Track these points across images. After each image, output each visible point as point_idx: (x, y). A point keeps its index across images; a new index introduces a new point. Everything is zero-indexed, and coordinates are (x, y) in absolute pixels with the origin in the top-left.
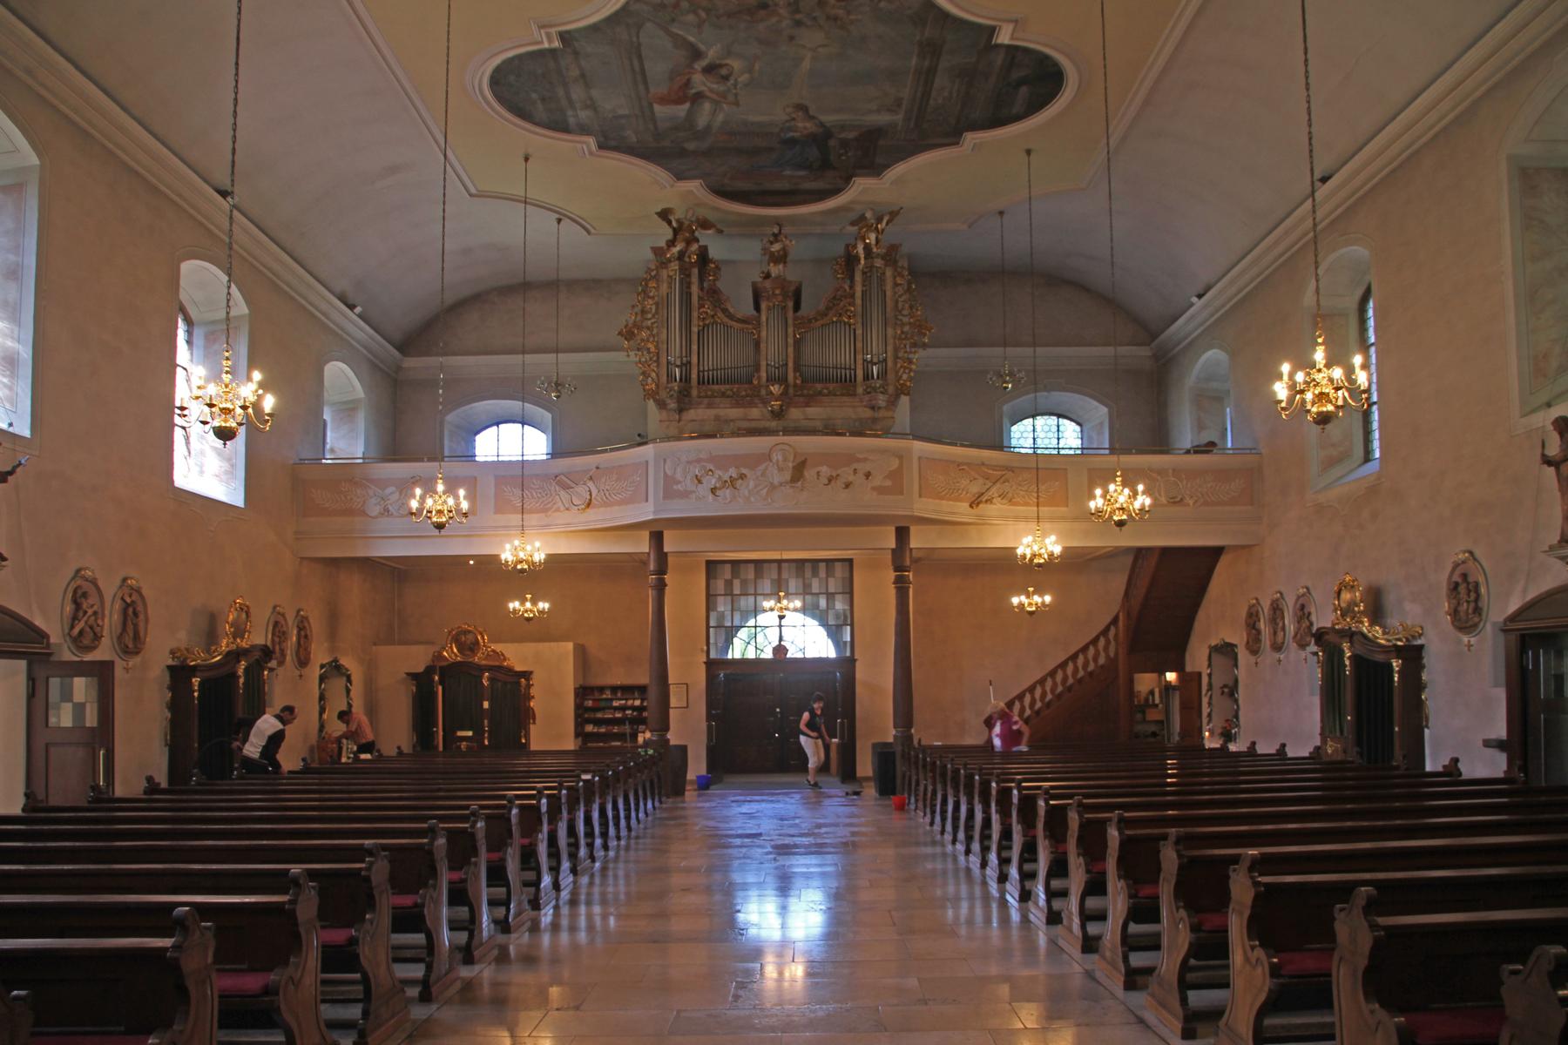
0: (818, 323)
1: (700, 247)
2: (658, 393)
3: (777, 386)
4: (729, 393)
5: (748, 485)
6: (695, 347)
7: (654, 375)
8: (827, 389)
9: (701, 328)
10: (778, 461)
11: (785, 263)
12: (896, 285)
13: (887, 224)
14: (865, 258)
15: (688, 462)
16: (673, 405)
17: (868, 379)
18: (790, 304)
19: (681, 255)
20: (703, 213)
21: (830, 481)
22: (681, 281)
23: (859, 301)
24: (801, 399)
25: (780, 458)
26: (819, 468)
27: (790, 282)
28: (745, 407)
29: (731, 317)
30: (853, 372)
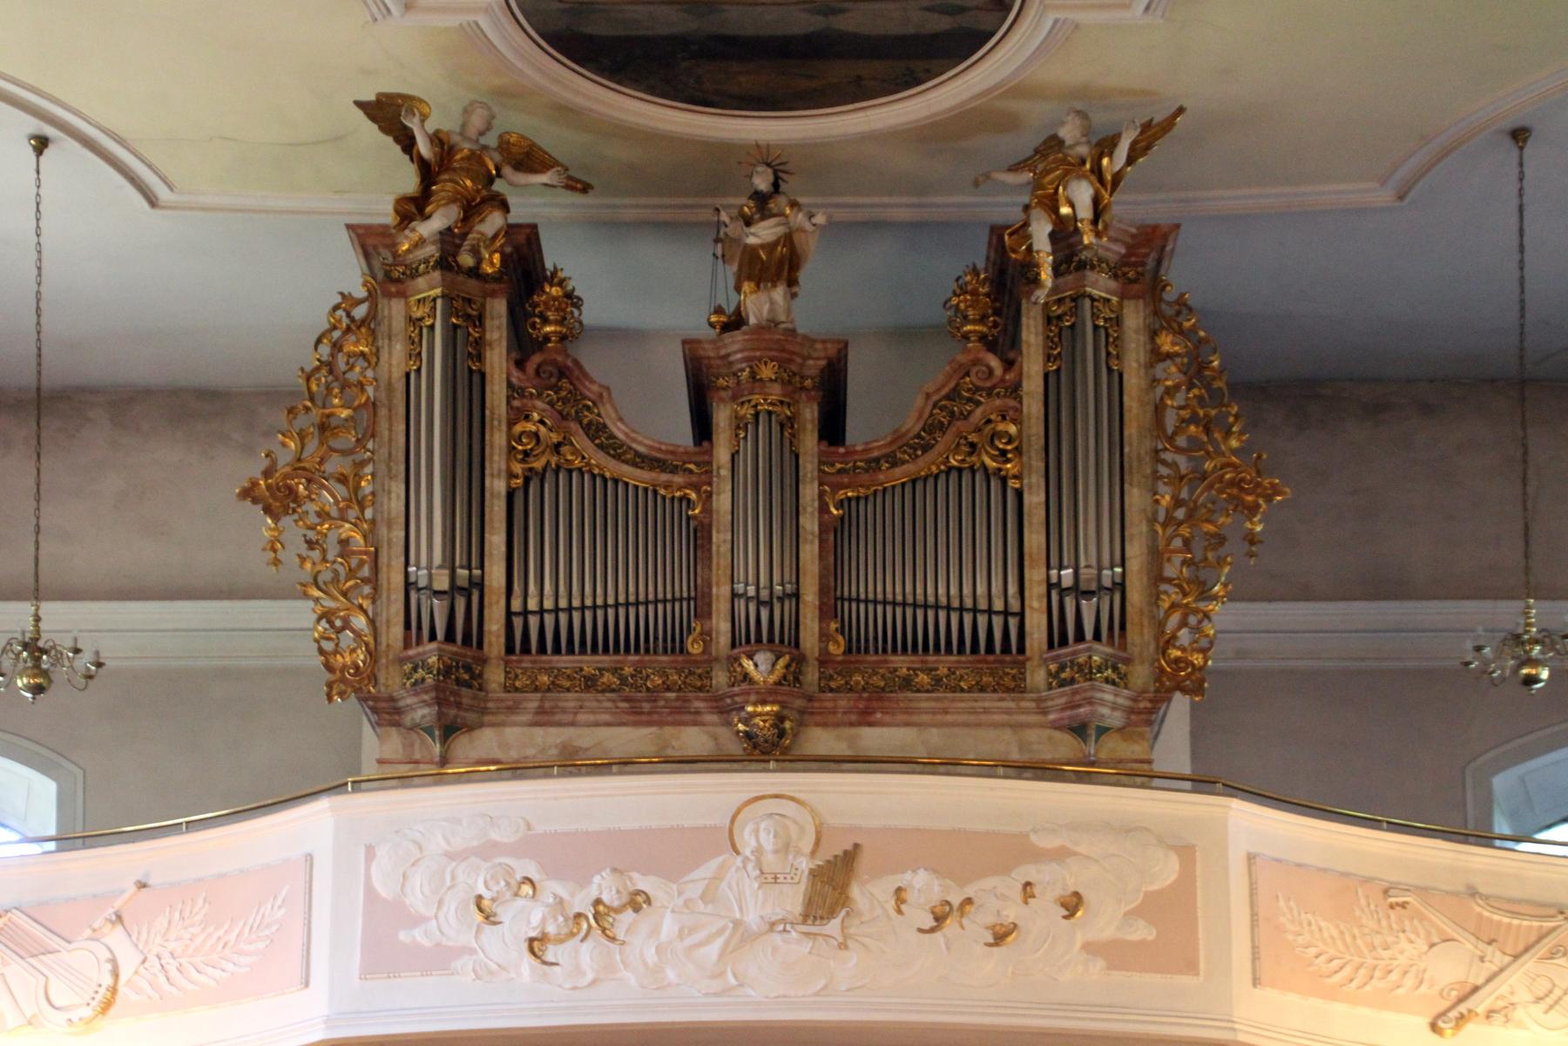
0: (898, 471)
1: (511, 230)
2: (373, 679)
3: (763, 658)
4: (608, 678)
5: (655, 931)
6: (496, 540)
7: (360, 622)
8: (929, 671)
10: (759, 851)
11: (792, 282)
12: (1157, 356)
13: (1130, 160)
14: (1057, 272)
15: (451, 856)
16: (422, 712)
17: (1064, 642)
18: (810, 413)
19: (450, 241)
20: (519, 123)
21: (940, 919)
22: (452, 332)
23: (1033, 405)
24: (844, 702)
25: (768, 842)
26: (905, 879)
27: (810, 341)
28: (660, 724)
29: (615, 449)
30: (1013, 623)
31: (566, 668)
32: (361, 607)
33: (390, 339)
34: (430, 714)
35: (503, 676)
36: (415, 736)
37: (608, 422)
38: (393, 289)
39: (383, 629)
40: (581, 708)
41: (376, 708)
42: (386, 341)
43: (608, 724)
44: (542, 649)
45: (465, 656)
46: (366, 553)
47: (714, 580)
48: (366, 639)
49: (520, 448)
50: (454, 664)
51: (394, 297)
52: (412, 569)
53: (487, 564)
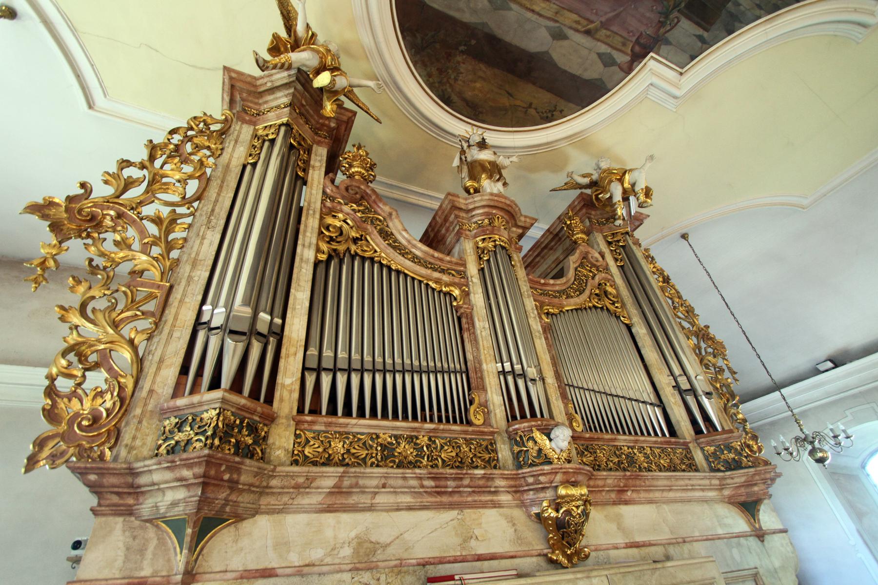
2: (116, 435)
4: (405, 449)
6: (300, 296)
9: (323, 257)
31: (362, 434)
32: (131, 342)
33: (236, 141)
34: (184, 500)
35: (292, 437)
36: (151, 532)
37: (394, 232)
38: (247, 118)
39: (150, 368)
40: (384, 486)
41: (101, 486)
42: (232, 143)
43: (410, 508)
44: (332, 410)
45: (253, 412)
46: (159, 287)
47: (483, 357)
48: (122, 380)
49: (327, 233)
50: (238, 422)
51: (247, 123)
52: (207, 308)
53: (289, 315)
